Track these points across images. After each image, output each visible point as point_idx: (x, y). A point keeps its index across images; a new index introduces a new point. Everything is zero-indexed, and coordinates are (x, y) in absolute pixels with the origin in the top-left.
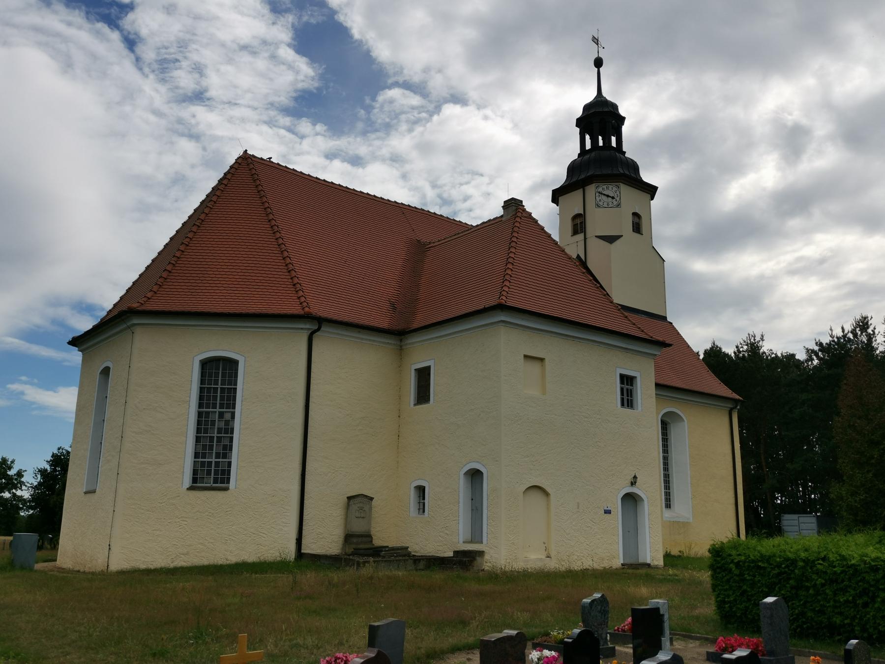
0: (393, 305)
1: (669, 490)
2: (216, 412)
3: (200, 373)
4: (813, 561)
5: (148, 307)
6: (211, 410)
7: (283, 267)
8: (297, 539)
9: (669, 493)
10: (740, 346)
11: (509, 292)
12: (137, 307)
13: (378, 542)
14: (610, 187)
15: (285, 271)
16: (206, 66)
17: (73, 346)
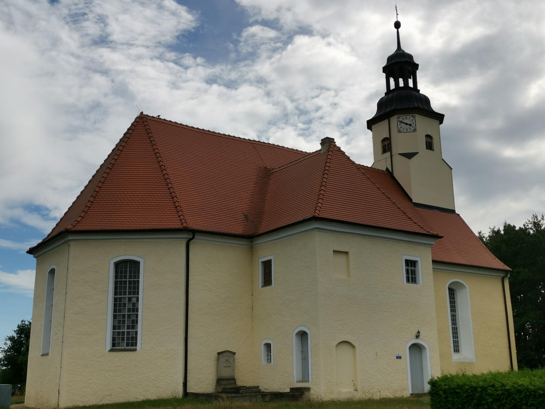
0: (246, 216)
1: (458, 338)
2: (126, 297)
3: (115, 271)
4: (487, 388)
5: (78, 228)
6: (123, 296)
7: (168, 195)
8: (183, 383)
9: (458, 341)
10: (526, 225)
11: (321, 211)
12: (71, 228)
13: (239, 383)
14: (408, 117)
15: (170, 197)
16: (107, 17)
17: (30, 254)
